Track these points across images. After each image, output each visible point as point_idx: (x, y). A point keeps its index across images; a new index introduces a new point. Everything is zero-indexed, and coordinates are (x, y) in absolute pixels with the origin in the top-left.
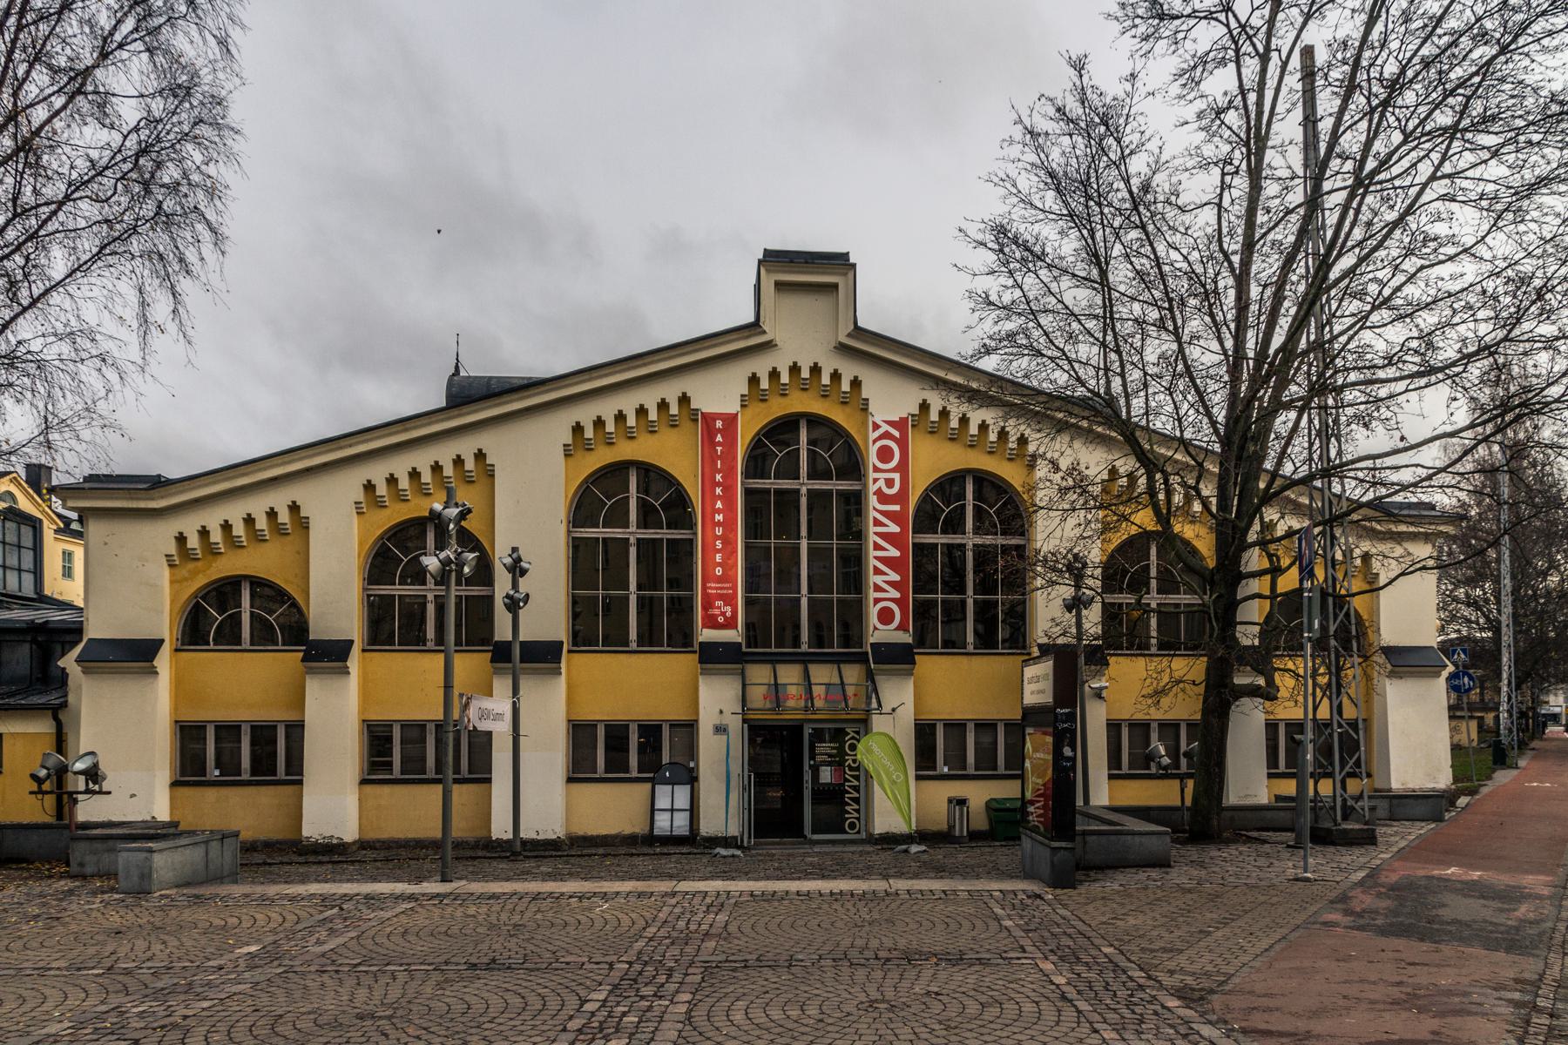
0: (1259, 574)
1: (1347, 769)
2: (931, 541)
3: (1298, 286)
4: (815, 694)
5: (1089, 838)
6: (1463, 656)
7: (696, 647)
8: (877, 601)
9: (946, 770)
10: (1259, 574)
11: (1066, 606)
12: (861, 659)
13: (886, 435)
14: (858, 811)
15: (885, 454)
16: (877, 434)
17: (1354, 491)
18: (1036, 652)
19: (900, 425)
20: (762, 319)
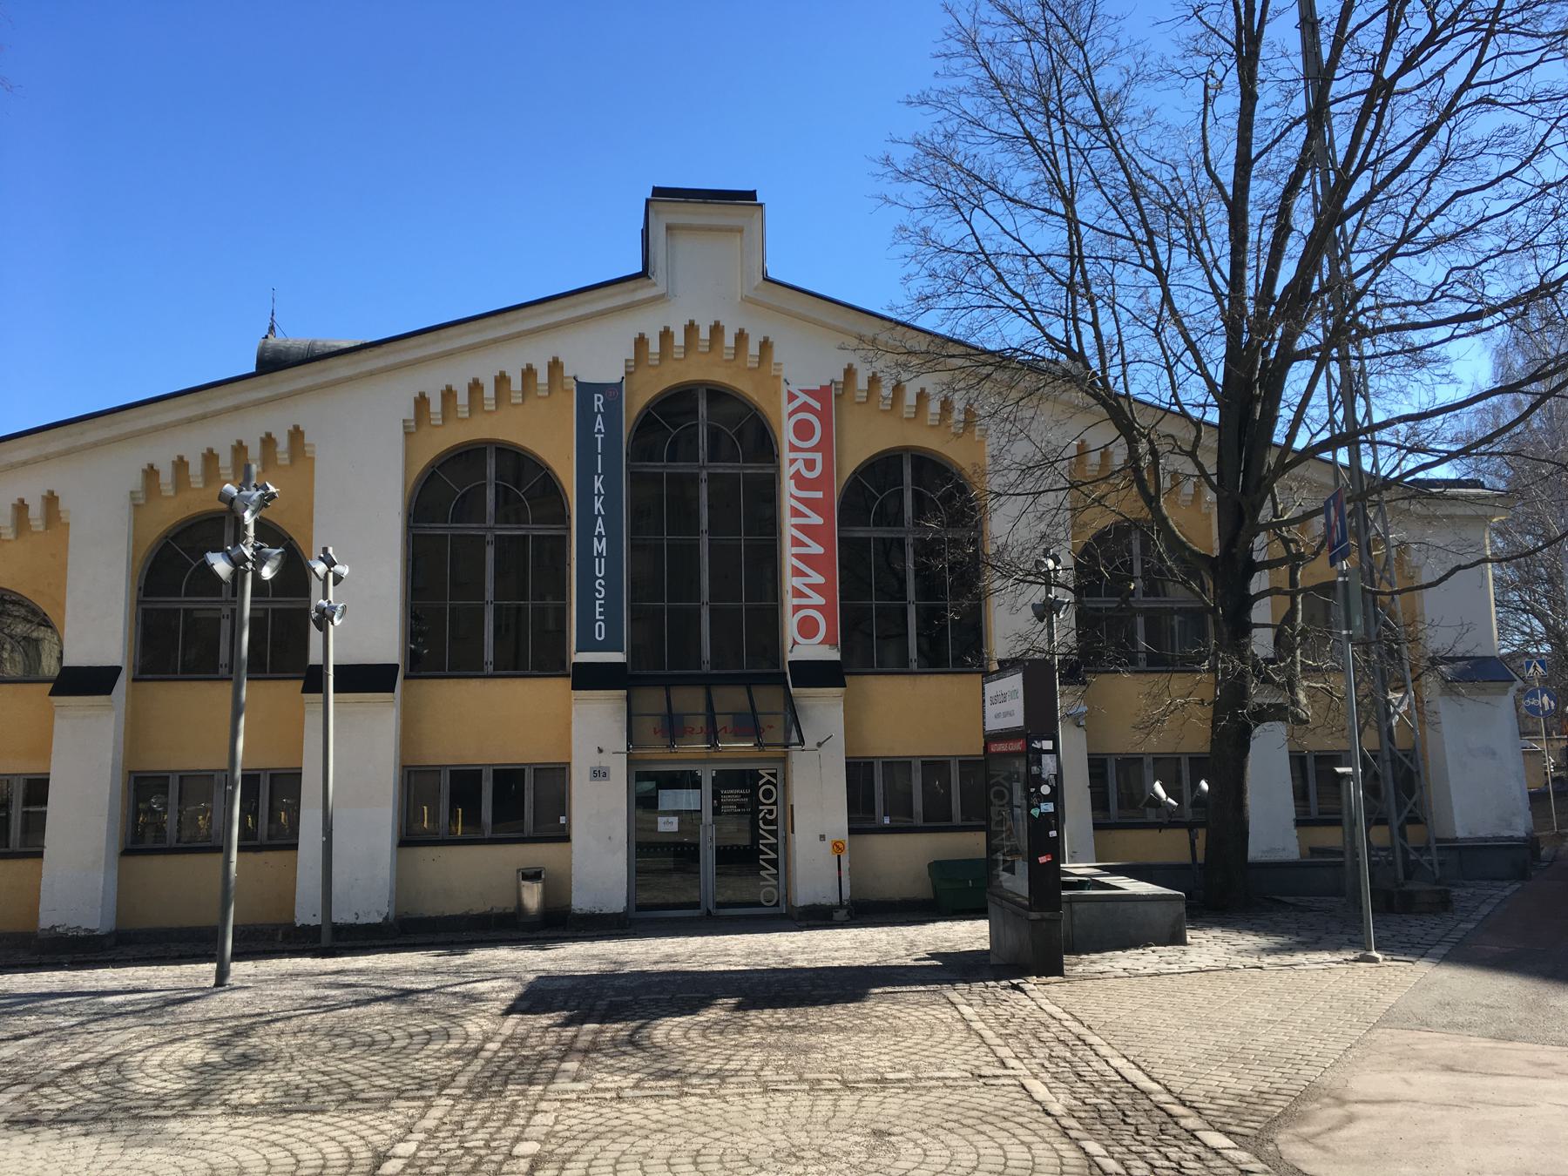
0: (1270, 565)
1: (1405, 812)
2: (862, 535)
3: (1303, 221)
4: (719, 727)
5: (1077, 906)
6: (1540, 669)
7: (570, 670)
8: (797, 608)
9: (887, 821)
10: (1270, 565)
11: (1036, 615)
12: (779, 679)
13: (805, 407)
14: (776, 877)
15: (803, 430)
16: (791, 407)
17: (1388, 463)
18: (995, 667)
19: (821, 394)
20: (651, 269)
